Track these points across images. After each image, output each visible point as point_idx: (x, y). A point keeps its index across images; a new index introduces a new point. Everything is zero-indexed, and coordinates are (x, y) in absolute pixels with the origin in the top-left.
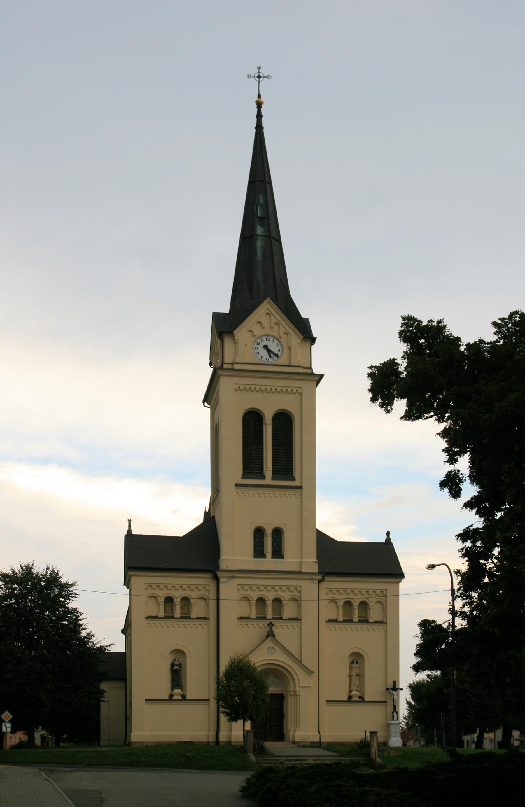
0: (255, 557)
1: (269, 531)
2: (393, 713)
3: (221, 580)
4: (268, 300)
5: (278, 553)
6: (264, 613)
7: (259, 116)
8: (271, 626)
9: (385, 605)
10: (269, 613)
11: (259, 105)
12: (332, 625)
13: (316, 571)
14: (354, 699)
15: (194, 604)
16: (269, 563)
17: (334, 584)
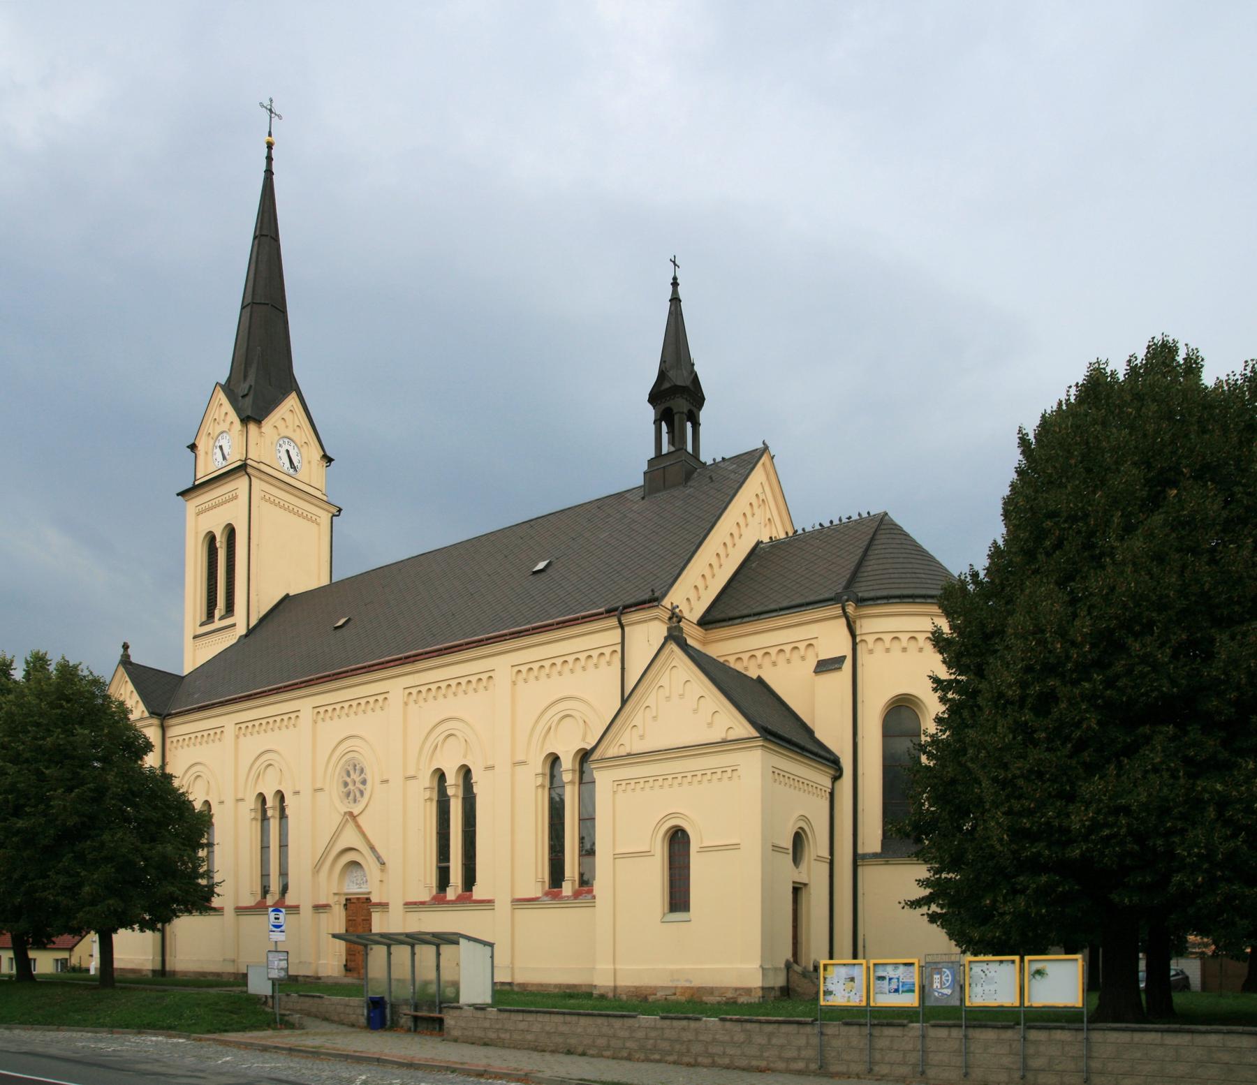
7: (269, 159)
11: (270, 146)
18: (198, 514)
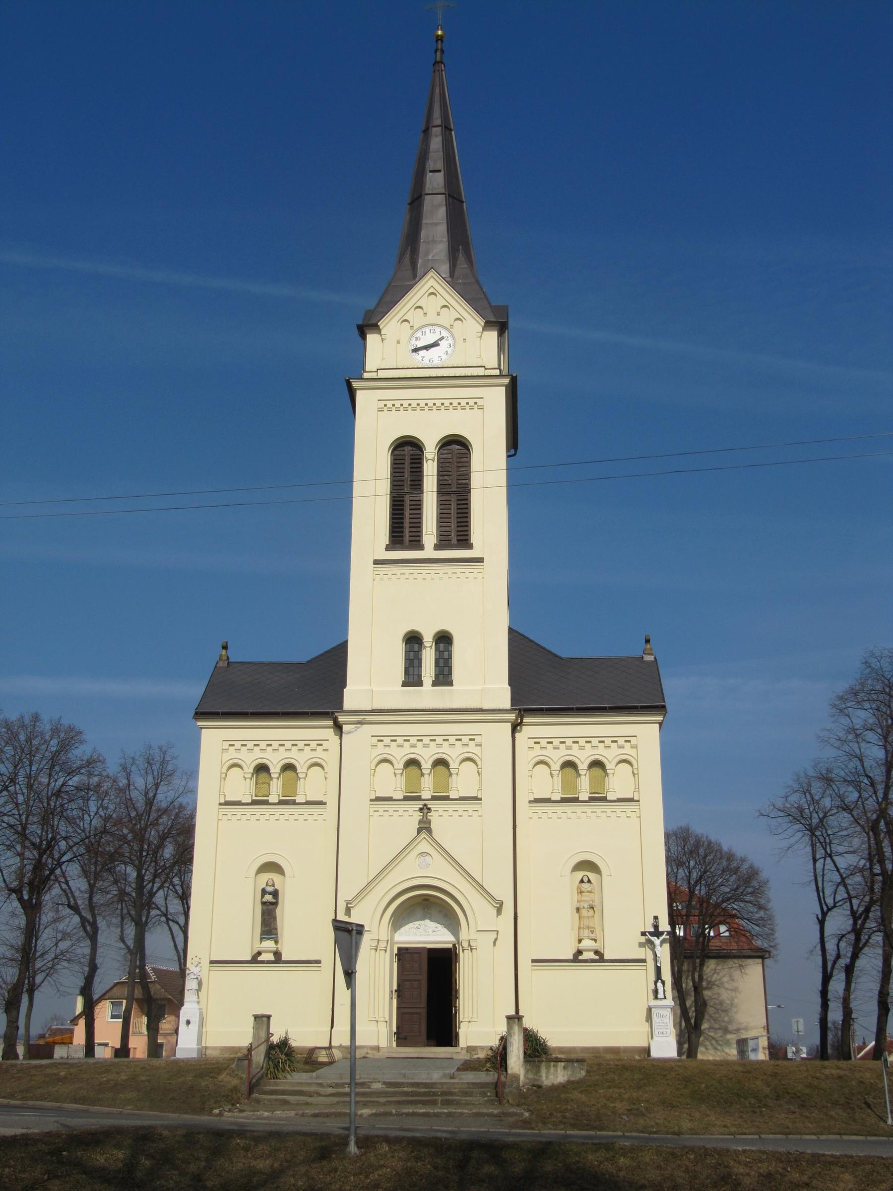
0: (405, 684)
1: (428, 638)
2: (656, 983)
3: (345, 728)
4: (432, 273)
5: (444, 677)
6: (575, 788)
8: (426, 811)
9: (635, 766)
10: (426, 789)
12: (541, 808)
13: (508, 705)
14: (264, 957)
15: (612, 772)
16: (428, 695)
17: (537, 729)
18: (380, 410)
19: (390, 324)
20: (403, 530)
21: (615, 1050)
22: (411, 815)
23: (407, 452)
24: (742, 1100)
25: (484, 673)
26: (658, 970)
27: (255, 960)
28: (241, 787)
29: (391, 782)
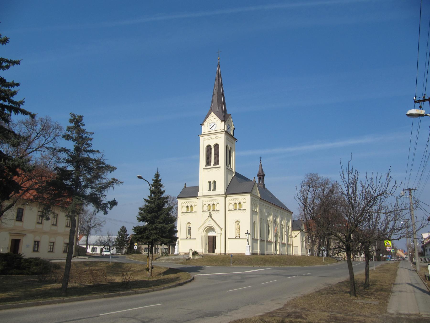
5: (215, 189)
16: (212, 192)
17: (229, 197)
19: (206, 124)
20: (208, 163)
21: (238, 253)
22: (208, 214)
23: (209, 147)
24: (37, 182)
25: (221, 188)
26: (248, 240)
27: (187, 239)
28: (184, 210)
29: (206, 208)
